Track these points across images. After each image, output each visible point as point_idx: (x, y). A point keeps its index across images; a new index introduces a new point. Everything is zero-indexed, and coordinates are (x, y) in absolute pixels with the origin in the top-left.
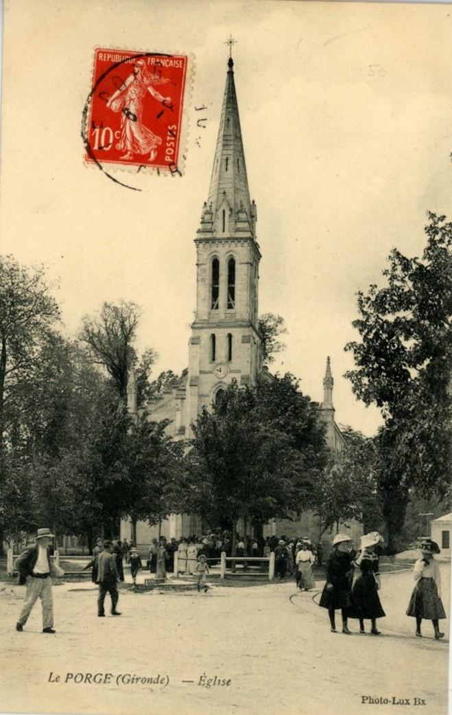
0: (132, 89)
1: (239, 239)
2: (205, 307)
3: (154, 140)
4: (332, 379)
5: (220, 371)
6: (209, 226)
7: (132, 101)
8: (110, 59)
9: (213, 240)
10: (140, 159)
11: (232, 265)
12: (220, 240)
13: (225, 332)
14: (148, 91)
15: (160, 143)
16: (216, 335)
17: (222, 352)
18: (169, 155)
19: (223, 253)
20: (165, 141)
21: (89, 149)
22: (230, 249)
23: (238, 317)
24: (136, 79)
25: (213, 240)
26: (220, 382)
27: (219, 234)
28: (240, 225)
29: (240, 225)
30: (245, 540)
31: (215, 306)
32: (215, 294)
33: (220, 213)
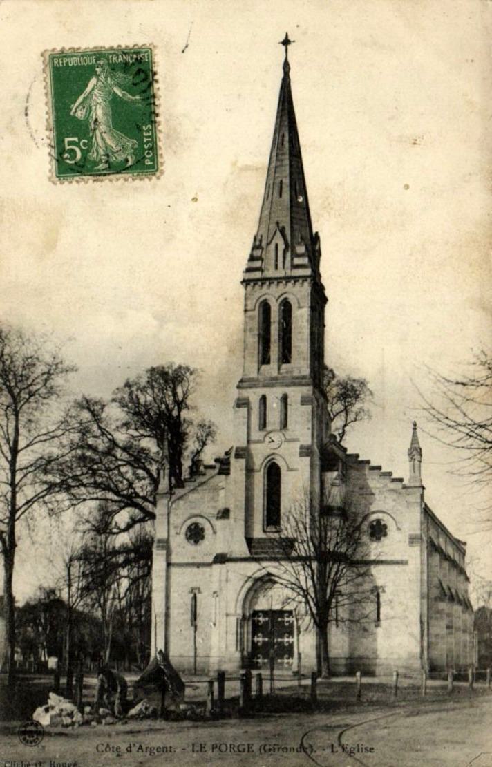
0: (96, 91)
1: (296, 279)
2: (412, 475)
3: (129, 144)
4: (420, 449)
5: (273, 441)
6: (257, 264)
7: (98, 106)
8: (67, 63)
9: (263, 281)
10: (118, 169)
11: (286, 308)
12: (271, 280)
13: (274, 395)
14: (114, 92)
15: (136, 146)
16: (267, 396)
17: (274, 417)
18: (149, 158)
19: (273, 295)
20: (141, 143)
21: (60, 160)
22: (285, 290)
23: (296, 374)
24: (98, 80)
25: (263, 281)
26: (273, 454)
27: (271, 273)
28: (297, 261)
29: (297, 261)
30: (81, 427)
31: (265, 360)
32: (265, 340)
33: (272, 246)
